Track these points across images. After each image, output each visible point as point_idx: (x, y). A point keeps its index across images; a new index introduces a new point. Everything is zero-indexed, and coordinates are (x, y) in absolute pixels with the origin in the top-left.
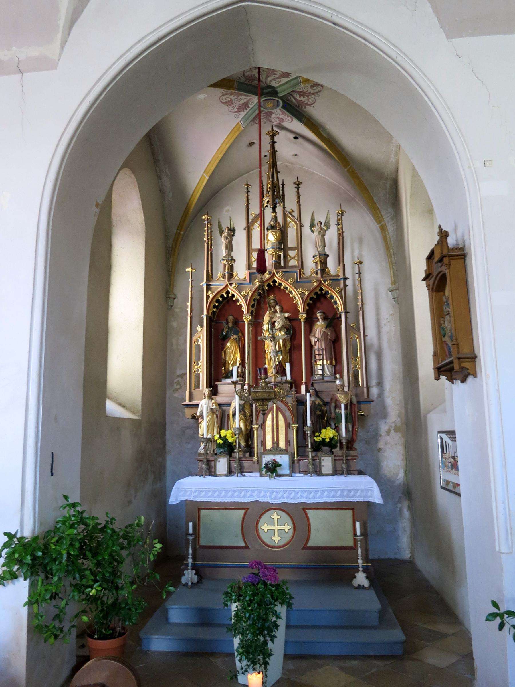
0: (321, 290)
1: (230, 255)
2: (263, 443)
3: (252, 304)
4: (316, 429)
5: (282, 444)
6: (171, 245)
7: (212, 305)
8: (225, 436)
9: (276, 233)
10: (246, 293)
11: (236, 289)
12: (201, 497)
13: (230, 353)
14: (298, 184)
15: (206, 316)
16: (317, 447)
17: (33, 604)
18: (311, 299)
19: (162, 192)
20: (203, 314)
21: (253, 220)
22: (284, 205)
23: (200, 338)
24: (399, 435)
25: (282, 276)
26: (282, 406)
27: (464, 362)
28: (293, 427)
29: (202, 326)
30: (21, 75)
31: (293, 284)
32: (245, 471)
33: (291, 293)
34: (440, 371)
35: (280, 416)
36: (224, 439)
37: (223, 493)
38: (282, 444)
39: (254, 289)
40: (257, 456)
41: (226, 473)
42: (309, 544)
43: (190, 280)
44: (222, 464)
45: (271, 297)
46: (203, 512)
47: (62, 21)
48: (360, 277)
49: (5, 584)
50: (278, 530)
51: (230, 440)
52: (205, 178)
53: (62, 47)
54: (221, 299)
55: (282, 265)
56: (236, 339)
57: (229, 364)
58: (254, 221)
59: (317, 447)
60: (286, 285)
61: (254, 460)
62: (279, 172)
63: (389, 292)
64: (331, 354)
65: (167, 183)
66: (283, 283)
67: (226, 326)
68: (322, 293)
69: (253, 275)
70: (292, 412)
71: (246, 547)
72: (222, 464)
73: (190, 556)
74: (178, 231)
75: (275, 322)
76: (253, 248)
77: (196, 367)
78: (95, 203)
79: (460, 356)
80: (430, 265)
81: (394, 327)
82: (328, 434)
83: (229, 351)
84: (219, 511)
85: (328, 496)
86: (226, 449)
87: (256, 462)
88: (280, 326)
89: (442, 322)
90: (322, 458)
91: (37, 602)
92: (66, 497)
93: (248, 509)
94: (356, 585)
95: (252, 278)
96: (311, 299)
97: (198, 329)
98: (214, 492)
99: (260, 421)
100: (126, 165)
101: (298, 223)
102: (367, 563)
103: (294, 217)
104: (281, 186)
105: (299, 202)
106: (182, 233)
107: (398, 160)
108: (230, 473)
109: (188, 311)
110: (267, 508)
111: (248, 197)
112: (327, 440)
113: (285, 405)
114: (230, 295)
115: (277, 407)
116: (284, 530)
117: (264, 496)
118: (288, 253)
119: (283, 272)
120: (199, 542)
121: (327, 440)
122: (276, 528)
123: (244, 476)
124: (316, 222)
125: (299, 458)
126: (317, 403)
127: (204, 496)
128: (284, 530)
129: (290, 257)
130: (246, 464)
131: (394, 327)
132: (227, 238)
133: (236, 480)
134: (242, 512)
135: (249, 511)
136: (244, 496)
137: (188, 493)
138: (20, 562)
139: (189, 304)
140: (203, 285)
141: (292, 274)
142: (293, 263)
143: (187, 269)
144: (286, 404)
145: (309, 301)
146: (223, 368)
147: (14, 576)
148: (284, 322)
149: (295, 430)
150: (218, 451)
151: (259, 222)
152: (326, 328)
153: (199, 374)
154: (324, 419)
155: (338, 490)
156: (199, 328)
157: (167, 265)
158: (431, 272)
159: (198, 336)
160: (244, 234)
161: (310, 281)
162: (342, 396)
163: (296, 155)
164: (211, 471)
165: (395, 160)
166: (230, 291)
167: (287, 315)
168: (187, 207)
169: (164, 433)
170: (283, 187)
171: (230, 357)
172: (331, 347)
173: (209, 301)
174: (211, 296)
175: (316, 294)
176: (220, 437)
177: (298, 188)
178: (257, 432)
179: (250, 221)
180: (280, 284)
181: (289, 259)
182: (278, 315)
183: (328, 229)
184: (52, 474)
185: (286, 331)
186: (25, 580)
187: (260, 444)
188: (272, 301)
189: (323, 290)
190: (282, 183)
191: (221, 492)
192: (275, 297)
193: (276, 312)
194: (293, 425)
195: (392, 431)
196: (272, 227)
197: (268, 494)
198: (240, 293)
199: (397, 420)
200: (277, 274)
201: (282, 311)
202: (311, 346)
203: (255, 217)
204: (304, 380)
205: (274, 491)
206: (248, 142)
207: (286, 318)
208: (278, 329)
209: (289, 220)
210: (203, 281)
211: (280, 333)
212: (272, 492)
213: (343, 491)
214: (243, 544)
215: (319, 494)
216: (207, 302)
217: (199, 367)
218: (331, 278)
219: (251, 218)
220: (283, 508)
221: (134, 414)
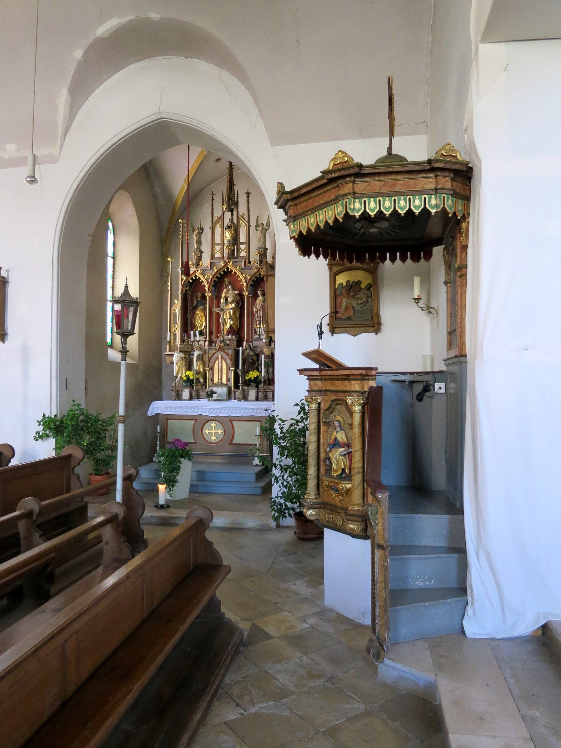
1: (200, 248)
2: (212, 380)
3: (212, 285)
4: (245, 372)
5: (224, 381)
8: (189, 375)
9: (231, 232)
10: (208, 277)
11: (201, 274)
12: (168, 412)
13: (198, 320)
14: (248, 194)
15: (181, 293)
16: (248, 383)
17: (57, 449)
18: (253, 281)
19: (155, 196)
20: (179, 291)
21: (216, 222)
22: (238, 210)
23: (177, 308)
25: (233, 264)
26: (225, 356)
28: (231, 370)
29: (178, 300)
30: (39, 166)
31: (240, 271)
32: (201, 398)
33: (239, 277)
35: (224, 363)
36: (188, 377)
37: (181, 410)
38: (224, 381)
39: (213, 274)
41: (188, 398)
42: (234, 442)
43: (170, 267)
44: (186, 393)
45: (226, 280)
46: (169, 421)
47: (60, 132)
49: (44, 439)
50: (215, 433)
51: (191, 378)
52: (185, 186)
53: (61, 149)
54: (191, 281)
55: (236, 256)
56: (202, 309)
57: (197, 326)
58: (217, 222)
59: (248, 383)
60: (235, 271)
62: (235, 185)
65: (158, 189)
66: (233, 270)
67: (196, 300)
69: (213, 264)
70: (231, 360)
71: (195, 443)
72: (186, 393)
73: (158, 446)
75: (228, 297)
76: (216, 243)
77: (174, 329)
78: (88, 235)
79: (268, 330)
82: (253, 374)
83: (197, 317)
84: (180, 421)
85: (244, 412)
86: (189, 383)
88: (231, 300)
90: (250, 390)
91: (59, 448)
92: (74, 401)
93: (197, 420)
94: (255, 464)
95: (213, 265)
96: (253, 281)
97: (175, 302)
98: (175, 408)
99: (211, 365)
100: (122, 187)
101: (247, 224)
102: (268, 454)
103: (244, 219)
104: (236, 195)
105: (248, 208)
106: (171, 227)
108: (191, 398)
109: (168, 289)
110: (208, 420)
111: (212, 204)
112: (252, 378)
114: (197, 278)
116: (219, 433)
117: (205, 412)
118: (240, 246)
119: (233, 261)
120: (167, 440)
121: (252, 378)
122: (213, 431)
123: (200, 400)
124: (260, 223)
125: (235, 390)
126: (250, 354)
127: (170, 411)
128: (219, 433)
129: (241, 249)
132: (197, 235)
133: (195, 403)
134: (194, 421)
135: (197, 421)
136: (193, 412)
137: (160, 409)
138: (50, 429)
139: (169, 284)
140: (179, 271)
141: (240, 263)
142: (243, 254)
143: (168, 259)
144: (228, 354)
147: (48, 436)
148: (234, 297)
149: (233, 372)
150: (184, 384)
151: (220, 223)
153: (176, 333)
154: (255, 365)
155: (250, 409)
156: (176, 302)
157: (162, 251)
159: (176, 306)
160: (210, 231)
161: (252, 269)
162: (267, 350)
164: (178, 397)
166: (198, 275)
167: (236, 292)
168: (174, 207)
169: (160, 373)
170: (238, 197)
171: (198, 322)
173: (183, 282)
175: (256, 277)
176: (186, 376)
177: (248, 197)
179: (214, 222)
180: (232, 271)
181: (241, 251)
182: (230, 292)
184: (67, 390)
185: (236, 303)
186: (53, 438)
187: (210, 380)
188: (227, 282)
189: (261, 274)
190: (237, 193)
191: (179, 408)
192: (230, 280)
193: (229, 290)
194: (231, 369)
196: (229, 227)
197: (208, 410)
198: (204, 276)
200: (229, 263)
201: (234, 289)
202: (253, 315)
203: (217, 220)
204: (245, 339)
205: (211, 409)
206: (215, 159)
207: (236, 294)
208: (230, 302)
209: (241, 222)
210: (179, 268)
211: (232, 305)
212: (210, 409)
213: (253, 409)
214: (194, 441)
215: (239, 411)
216: (181, 283)
217: (176, 328)
219: (215, 220)
220: (216, 419)
221: (133, 360)
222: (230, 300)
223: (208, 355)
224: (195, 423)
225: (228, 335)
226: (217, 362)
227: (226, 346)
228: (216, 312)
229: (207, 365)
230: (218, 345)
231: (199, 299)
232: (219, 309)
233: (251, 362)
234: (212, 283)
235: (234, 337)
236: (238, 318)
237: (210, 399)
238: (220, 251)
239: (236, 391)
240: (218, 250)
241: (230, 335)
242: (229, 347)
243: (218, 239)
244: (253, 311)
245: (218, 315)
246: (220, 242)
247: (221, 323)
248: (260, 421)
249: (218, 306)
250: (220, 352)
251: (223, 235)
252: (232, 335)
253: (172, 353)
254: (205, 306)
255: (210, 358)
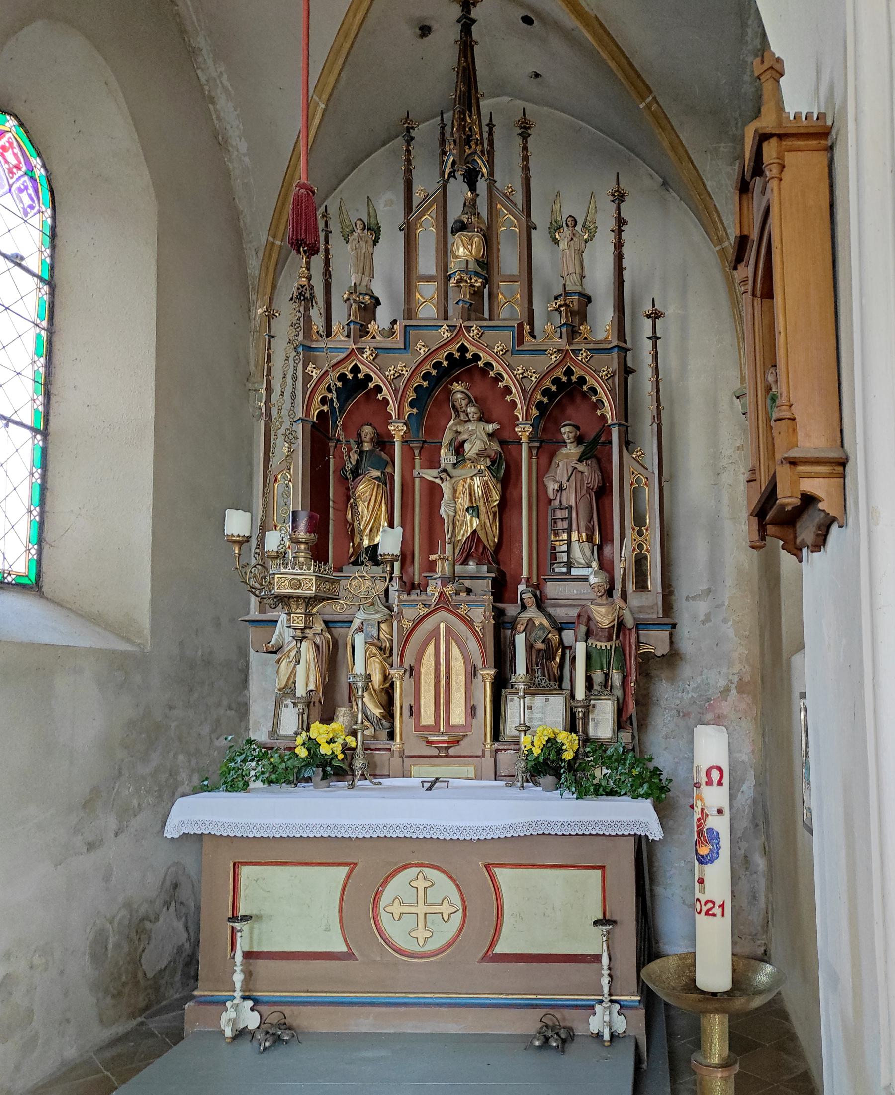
0: (569, 372)
2: (413, 711)
6: (257, 273)
7: (318, 398)
14: (525, 129)
24: (748, 699)
27: (810, 476)
34: (766, 525)
35: (455, 651)
40: (401, 739)
48: (655, 346)
56: (378, 478)
57: (361, 533)
61: (393, 748)
63: (735, 398)
64: (591, 519)
68: (570, 380)
70: (481, 642)
71: (348, 956)
74: (271, 239)
80: (745, 211)
81: (744, 474)
87: (396, 754)
89: (771, 379)
101: (524, 219)
103: (515, 205)
107: (761, 90)
113: (466, 624)
115: (448, 630)
126: (537, 623)
130: (381, 756)
131: (744, 474)
144: (468, 622)
145: (539, 397)
146: (351, 544)
152: (580, 460)
154: (554, 659)
158: (746, 233)
162: (603, 610)
163: (537, 75)
165: (753, 90)
167: (491, 428)
170: (491, 133)
172: (591, 502)
174: (316, 374)
175: (557, 381)
177: (525, 136)
178: (401, 685)
183: (591, 238)
185: (489, 463)
187: (406, 712)
188: (459, 395)
190: (488, 121)
195: (734, 692)
199: (744, 670)
204: (525, 573)
218: (591, 346)
222: (471, 450)
223: (399, 621)
224: (348, 877)
225: (465, 562)
226: (431, 649)
227: (464, 594)
228: (422, 478)
229: (396, 659)
230: (434, 589)
231: (367, 447)
232: (434, 472)
233: (540, 651)
234: (411, 395)
235: (485, 568)
236: (496, 509)
237: (393, 433)
238: (435, 302)
239: (501, 750)
240: (428, 296)
241: (471, 563)
242: (472, 597)
243: (427, 264)
244: (546, 487)
245: (433, 492)
246: (433, 272)
247: (444, 516)
248: (602, 868)
249: (433, 463)
250: (443, 614)
251: (444, 251)
252: (479, 563)
253: (270, 615)
254: (389, 470)
255: (405, 634)
